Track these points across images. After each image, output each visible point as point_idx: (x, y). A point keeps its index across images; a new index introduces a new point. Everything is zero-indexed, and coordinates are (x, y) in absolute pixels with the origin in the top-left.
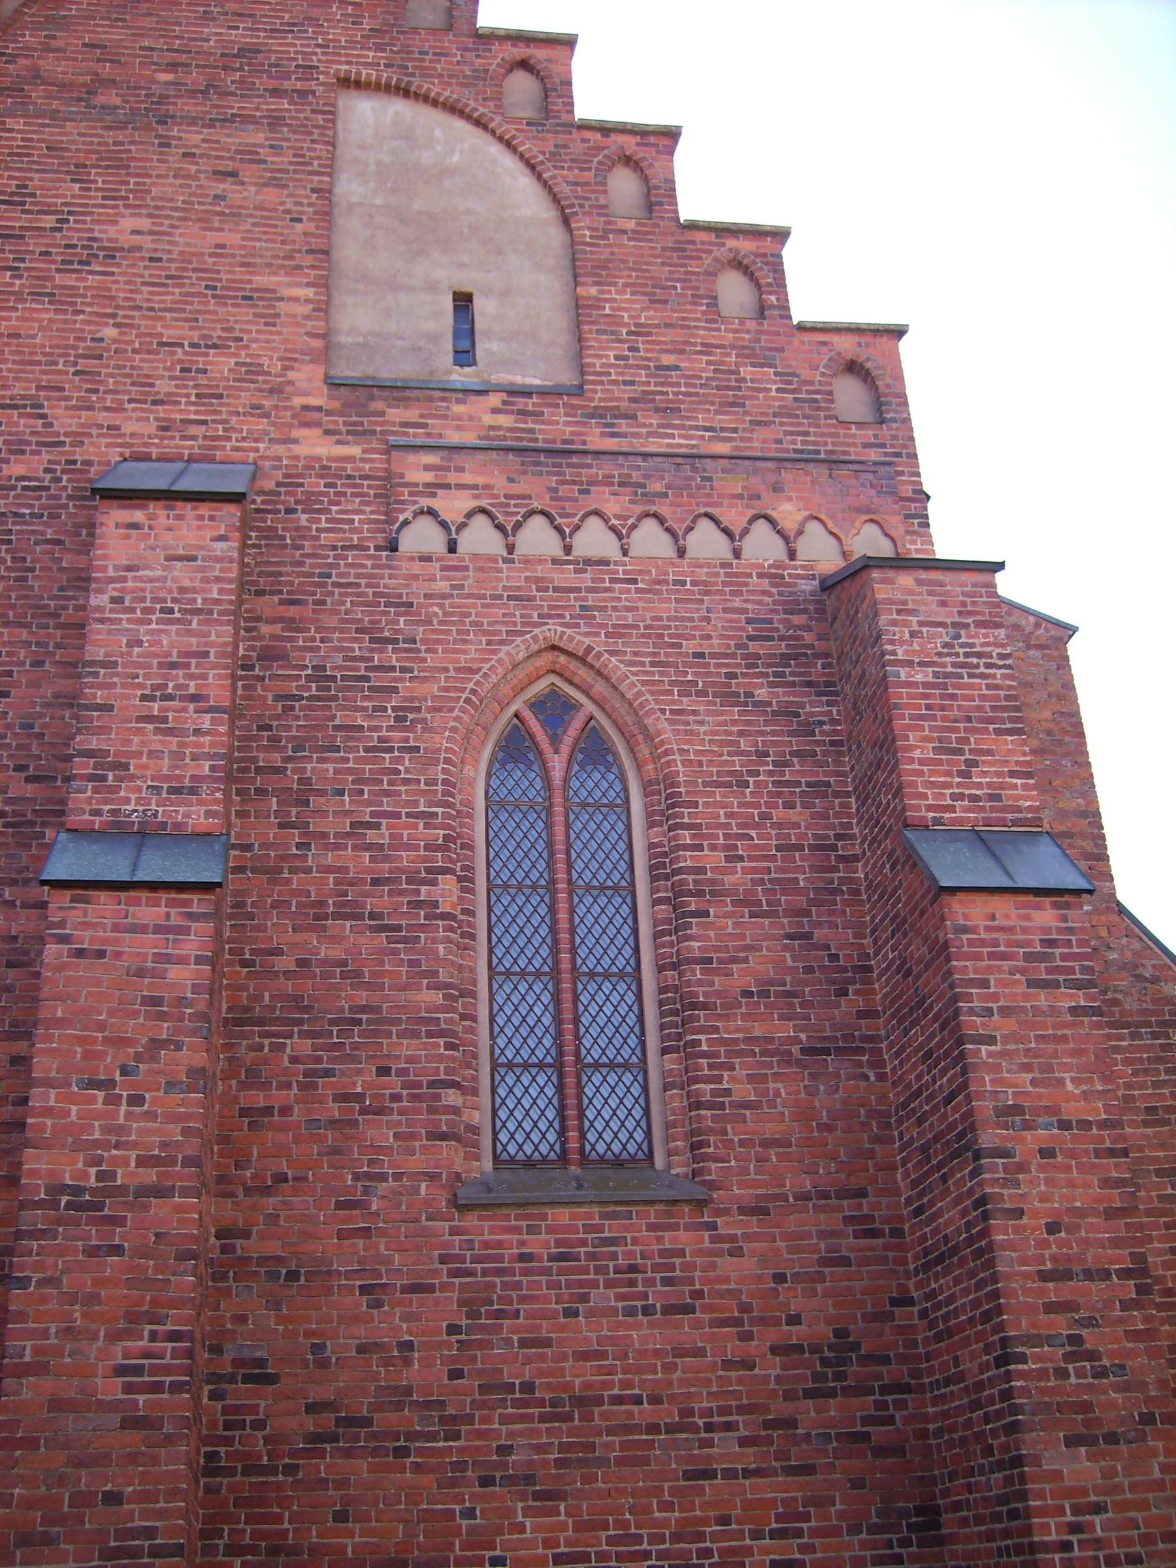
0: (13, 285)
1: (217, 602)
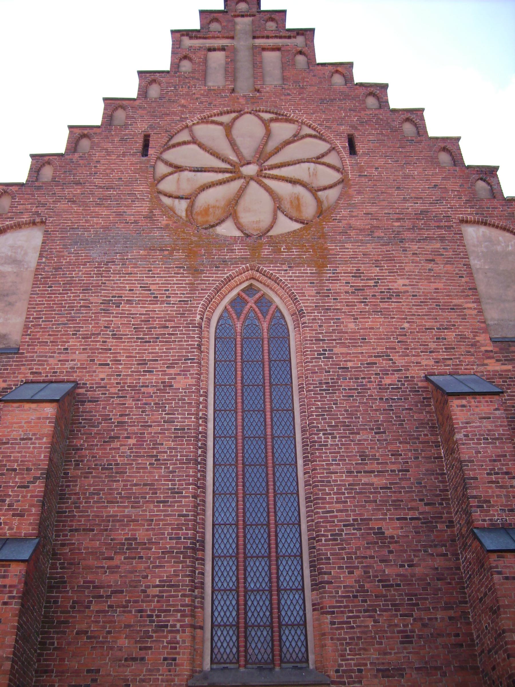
0: (365, 308)
1: (503, 435)
